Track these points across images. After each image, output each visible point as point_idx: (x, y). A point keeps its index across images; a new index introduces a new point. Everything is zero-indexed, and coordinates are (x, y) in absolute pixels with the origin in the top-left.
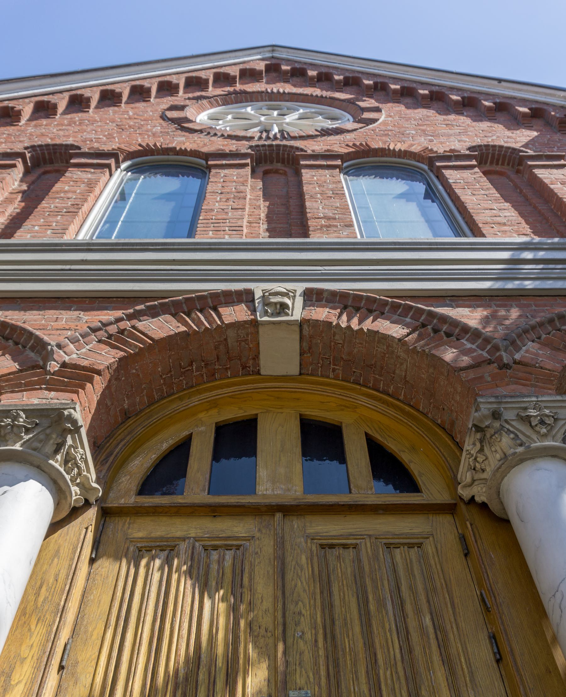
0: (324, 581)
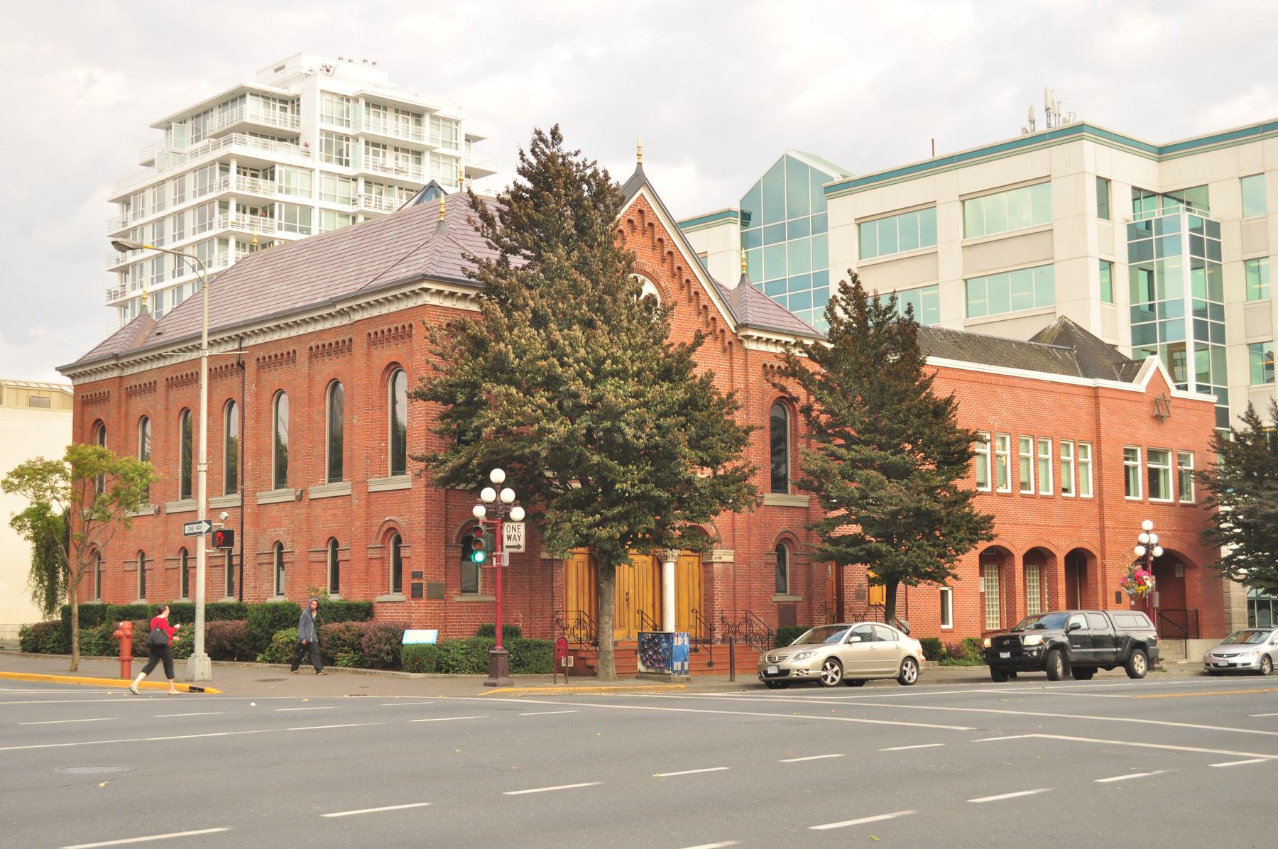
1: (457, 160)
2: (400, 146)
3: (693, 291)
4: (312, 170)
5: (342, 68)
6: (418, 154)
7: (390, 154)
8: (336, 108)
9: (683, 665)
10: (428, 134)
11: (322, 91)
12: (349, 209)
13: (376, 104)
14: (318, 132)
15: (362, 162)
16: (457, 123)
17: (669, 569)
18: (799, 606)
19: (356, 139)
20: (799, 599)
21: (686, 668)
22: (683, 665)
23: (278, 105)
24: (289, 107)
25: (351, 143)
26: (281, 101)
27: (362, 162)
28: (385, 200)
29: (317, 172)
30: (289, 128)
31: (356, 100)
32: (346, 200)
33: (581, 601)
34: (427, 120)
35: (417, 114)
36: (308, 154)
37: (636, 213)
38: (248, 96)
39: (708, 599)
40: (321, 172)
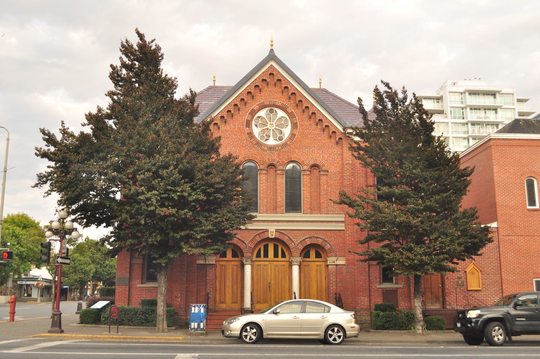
0: (275, 270)
1: (514, 109)
2: (486, 108)
3: (311, 112)
4: (448, 123)
5: (460, 83)
6: (495, 109)
7: (482, 112)
8: (458, 97)
9: (199, 325)
10: (499, 101)
11: (450, 92)
12: (465, 136)
13: (473, 93)
14: (449, 108)
15: (472, 116)
16: (513, 94)
17: (248, 269)
18: (399, 292)
19: (466, 108)
20: (401, 286)
21: (202, 326)
22: (199, 325)
23: (435, 101)
24: (440, 101)
25: (464, 110)
26: (437, 99)
27: (472, 116)
28: (482, 130)
29: (450, 123)
30: (440, 109)
31: (465, 93)
32: (465, 133)
33: (235, 287)
34: (497, 95)
35: (493, 94)
36: (446, 117)
37: (268, 75)
38: (423, 100)
39: (317, 284)
40: (452, 123)
